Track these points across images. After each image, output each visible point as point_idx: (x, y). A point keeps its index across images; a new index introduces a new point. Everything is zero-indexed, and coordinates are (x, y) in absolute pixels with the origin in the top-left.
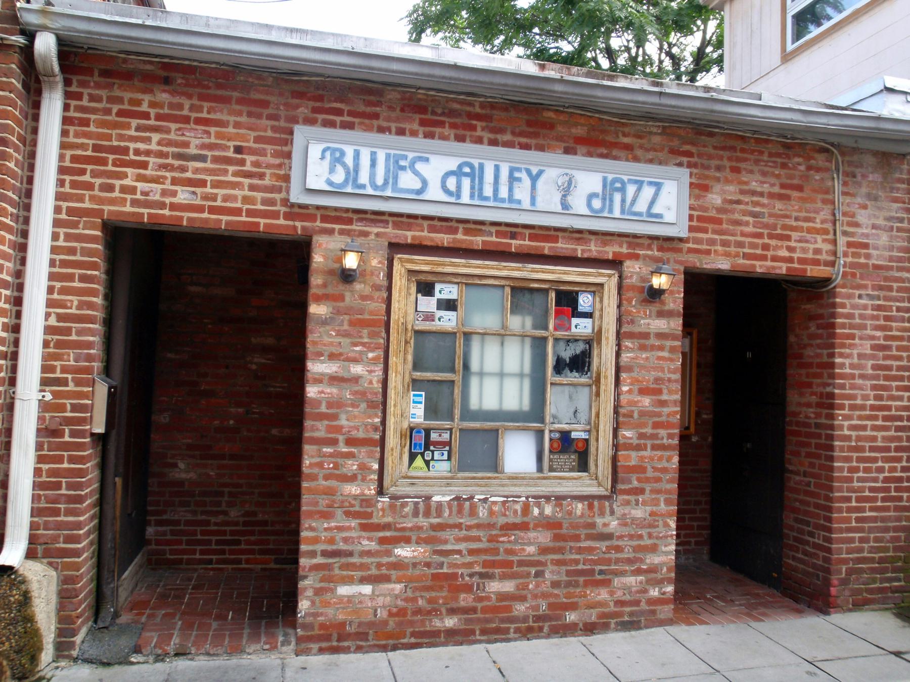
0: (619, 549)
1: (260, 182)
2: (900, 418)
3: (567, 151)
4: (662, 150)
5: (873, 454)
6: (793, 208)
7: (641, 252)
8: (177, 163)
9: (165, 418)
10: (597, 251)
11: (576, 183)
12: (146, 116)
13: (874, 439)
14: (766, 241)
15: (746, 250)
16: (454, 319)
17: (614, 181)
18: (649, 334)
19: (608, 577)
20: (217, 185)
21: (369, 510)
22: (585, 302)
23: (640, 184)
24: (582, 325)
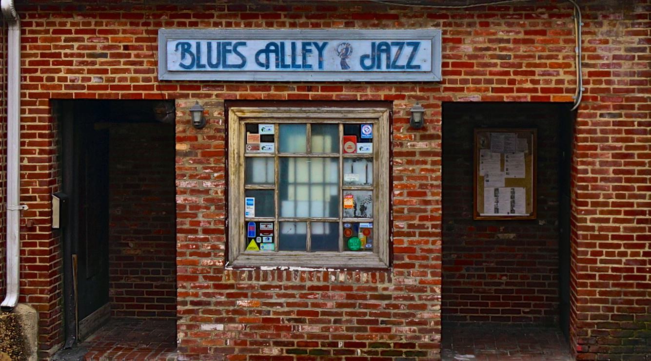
0: (396, 307)
1: (140, 67)
2: (643, 213)
3: (348, 25)
4: (421, 16)
5: (615, 242)
6: (536, 49)
7: (406, 94)
8: (89, 60)
9: (118, 211)
10: (372, 95)
11: (351, 48)
12: (69, 32)
13: (617, 229)
14: (512, 77)
15: (494, 86)
16: (273, 148)
17: (380, 45)
18: (415, 152)
19: (388, 326)
20: (115, 71)
21: (220, 275)
22: (366, 131)
23: (401, 45)
24: (267, 147)
